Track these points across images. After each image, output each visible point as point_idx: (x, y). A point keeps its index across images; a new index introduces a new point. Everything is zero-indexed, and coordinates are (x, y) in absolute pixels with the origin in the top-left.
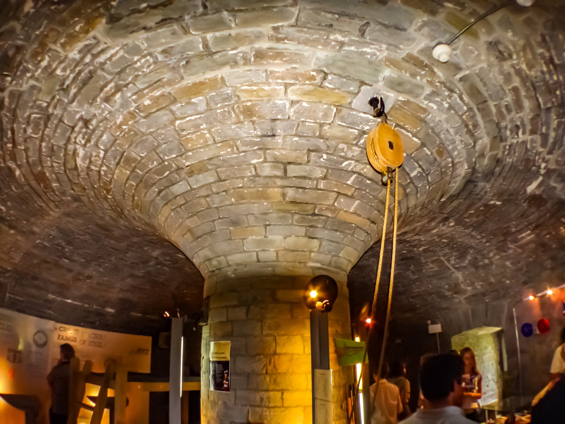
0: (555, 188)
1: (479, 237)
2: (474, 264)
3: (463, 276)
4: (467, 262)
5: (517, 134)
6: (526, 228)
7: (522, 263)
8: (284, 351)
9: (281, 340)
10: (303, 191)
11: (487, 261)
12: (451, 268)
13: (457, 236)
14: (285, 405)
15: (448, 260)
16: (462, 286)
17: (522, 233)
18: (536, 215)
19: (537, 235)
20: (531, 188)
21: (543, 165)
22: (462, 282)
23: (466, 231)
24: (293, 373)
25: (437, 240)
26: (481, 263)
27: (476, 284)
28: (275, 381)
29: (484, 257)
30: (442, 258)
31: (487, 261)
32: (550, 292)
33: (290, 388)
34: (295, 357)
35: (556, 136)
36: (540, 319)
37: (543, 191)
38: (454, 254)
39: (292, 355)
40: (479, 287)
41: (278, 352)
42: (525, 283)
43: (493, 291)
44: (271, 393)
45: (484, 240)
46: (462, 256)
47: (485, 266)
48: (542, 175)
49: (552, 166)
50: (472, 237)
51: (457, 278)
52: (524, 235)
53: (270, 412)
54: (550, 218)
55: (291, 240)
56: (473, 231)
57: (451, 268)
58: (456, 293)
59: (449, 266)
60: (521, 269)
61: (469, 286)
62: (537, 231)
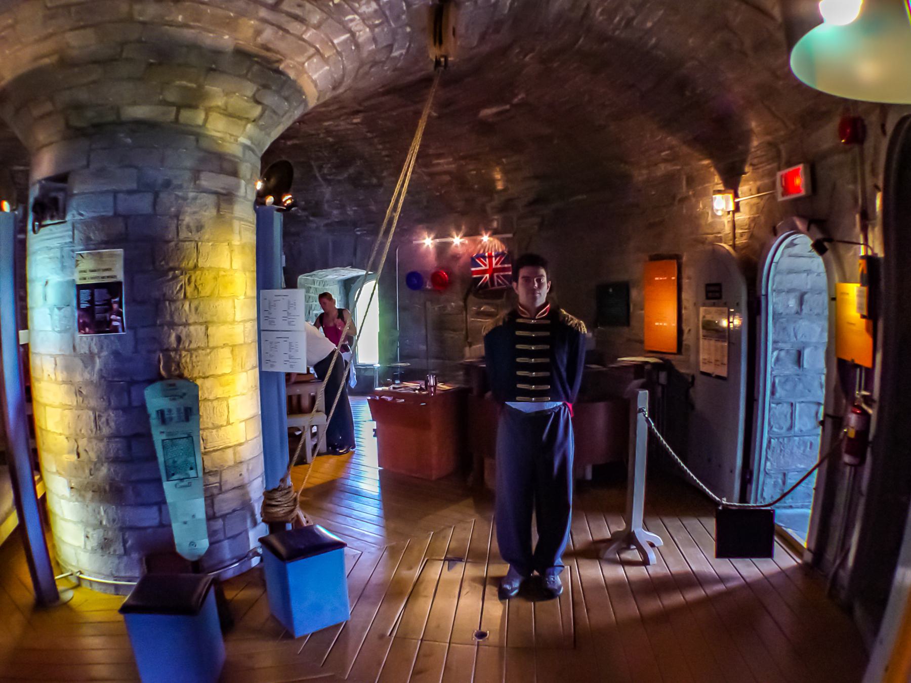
2: (355, 181)
8: (208, 265)
9: (205, 247)
10: (283, 36)
11: (375, 181)
12: (320, 178)
14: (211, 345)
15: (320, 168)
16: (326, 206)
22: (328, 201)
24: (219, 297)
26: (365, 182)
28: (196, 309)
30: (313, 163)
31: (375, 181)
33: (215, 318)
34: (222, 273)
36: (433, 271)
39: (219, 269)
41: (200, 265)
44: (192, 328)
45: (384, 153)
46: (343, 165)
52: (441, 161)
53: (191, 357)
57: (320, 178)
58: (314, 215)
59: (318, 175)
61: (337, 208)
62: (463, 162)
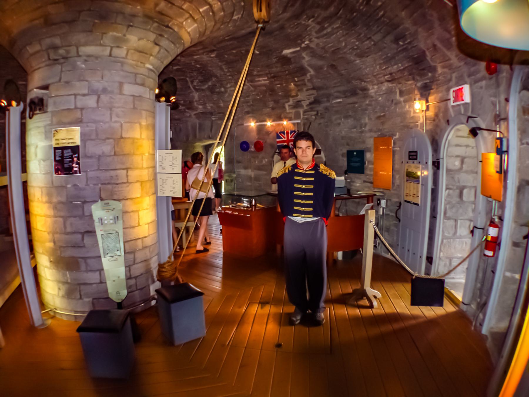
0: (304, 58)
1: (226, 70)
3: (199, 96)
4: (206, 86)
5: (309, 20)
6: (266, 75)
7: (251, 98)
11: (223, 89)
13: (209, 65)
15: (192, 82)
17: (260, 78)
18: (278, 69)
19: (271, 83)
20: (287, 52)
21: (307, 42)
22: (196, 101)
23: (220, 63)
25: (193, 64)
26: (217, 90)
27: (207, 105)
29: (222, 86)
30: (188, 79)
31: (223, 89)
32: (269, 124)
35: (330, 32)
36: (255, 141)
37: (294, 57)
38: (200, 78)
39: (133, 139)
40: (209, 107)
42: (248, 113)
43: (219, 113)
45: (228, 74)
46: (205, 80)
47: (219, 93)
48: (301, 47)
49: (312, 45)
50: (221, 69)
51: (193, 97)
52: (261, 79)
54: (287, 75)
55: (143, 43)
56: (224, 65)
59: (191, 86)
60: (248, 102)
